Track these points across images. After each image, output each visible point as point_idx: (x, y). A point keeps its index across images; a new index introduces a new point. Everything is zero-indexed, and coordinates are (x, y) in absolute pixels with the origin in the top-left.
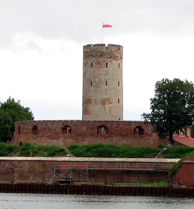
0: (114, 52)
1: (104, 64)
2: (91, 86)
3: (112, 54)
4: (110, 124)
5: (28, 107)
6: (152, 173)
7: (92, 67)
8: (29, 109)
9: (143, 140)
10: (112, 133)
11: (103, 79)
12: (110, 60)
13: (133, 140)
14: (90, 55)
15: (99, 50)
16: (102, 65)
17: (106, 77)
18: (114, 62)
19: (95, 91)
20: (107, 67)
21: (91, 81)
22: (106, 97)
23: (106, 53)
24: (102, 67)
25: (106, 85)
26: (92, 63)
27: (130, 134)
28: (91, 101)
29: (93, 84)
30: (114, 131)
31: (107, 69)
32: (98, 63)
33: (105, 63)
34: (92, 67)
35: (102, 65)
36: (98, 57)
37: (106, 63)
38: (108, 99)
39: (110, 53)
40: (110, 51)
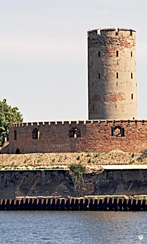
0: (126, 38)
12: (121, 48)
18: (126, 50)
20: (117, 56)
31: (117, 58)
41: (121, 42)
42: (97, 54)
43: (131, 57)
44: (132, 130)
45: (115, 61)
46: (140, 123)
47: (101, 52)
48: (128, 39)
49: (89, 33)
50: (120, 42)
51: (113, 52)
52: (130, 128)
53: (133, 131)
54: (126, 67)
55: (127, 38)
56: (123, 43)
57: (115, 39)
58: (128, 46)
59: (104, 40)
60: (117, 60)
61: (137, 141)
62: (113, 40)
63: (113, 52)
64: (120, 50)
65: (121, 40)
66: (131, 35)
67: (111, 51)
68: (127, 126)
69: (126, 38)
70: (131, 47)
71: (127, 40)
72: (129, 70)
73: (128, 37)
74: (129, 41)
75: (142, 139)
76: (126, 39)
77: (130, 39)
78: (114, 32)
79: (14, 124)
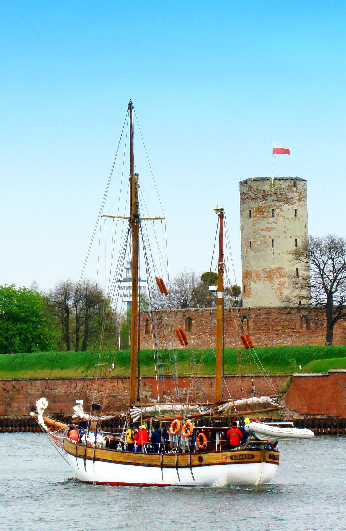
0: (286, 191)
1: (269, 212)
2: (249, 250)
3: (281, 194)
4: (256, 314)
5: (283, 267)
6: (36, 380)
7: (250, 217)
8: (304, 268)
9: (313, 338)
10: (33, 342)
11: (268, 237)
12: (278, 204)
13: (296, 338)
14: (247, 198)
15: (260, 188)
16: (265, 214)
17: (272, 233)
18: (286, 207)
19: (255, 257)
20: (273, 216)
21: (250, 242)
22: (273, 267)
23: (272, 193)
24: (265, 217)
25: (273, 247)
26: (250, 211)
27: (290, 328)
28: (251, 274)
29: (254, 246)
30: (262, 324)
31: (274, 220)
32: (260, 210)
33: (271, 210)
34: (250, 217)
35: (265, 214)
36: (258, 200)
37: (271, 209)
38: (277, 269)
39: (278, 193)
40: (278, 190)
41: (279, 197)
42: (248, 214)
43: (294, 217)
44: (263, 321)
45: (270, 223)
46: (274, 310)
47: (252, 211)
48: (290, 192)
49: (244, 183)
50: (277, 197)
51: (267, 211)
52: (261, 318)
53: (264, 322)
54: (287, 231)
55: (287, 191)
56: (282, 198)
57: (269, 193)
58: (290, 201)
59: (256, 195)
60: (273, 222)
61: (271, 336)
62: (267, 194)
63: (267, 211)
64: (278, 208)
65: (278, 193)
66: (295, 185)
67: (264, 210)
68: (257, 315)
69: (286, 191)
70: (296, 203)
71: (288, 194)
72: (292, 235)
73: (291, 188)
74: (291, 195)
75: (278, 333)
76: (286, 192)
77: (293, 192)
78: (269, 183)
79: (192, 388)
